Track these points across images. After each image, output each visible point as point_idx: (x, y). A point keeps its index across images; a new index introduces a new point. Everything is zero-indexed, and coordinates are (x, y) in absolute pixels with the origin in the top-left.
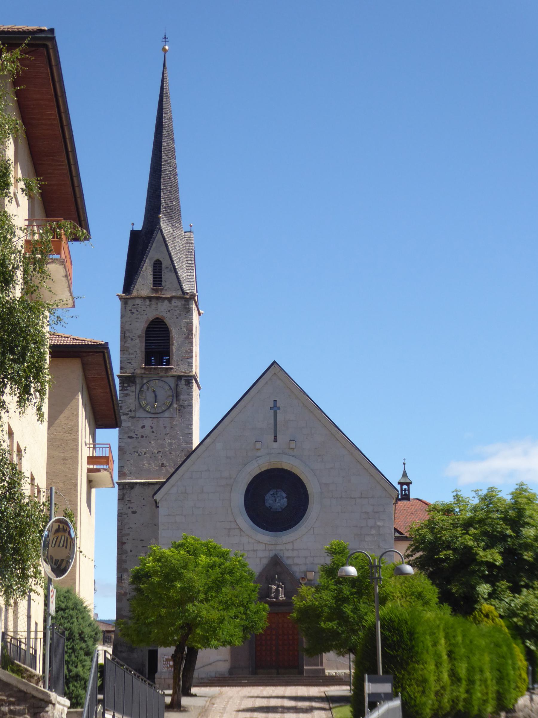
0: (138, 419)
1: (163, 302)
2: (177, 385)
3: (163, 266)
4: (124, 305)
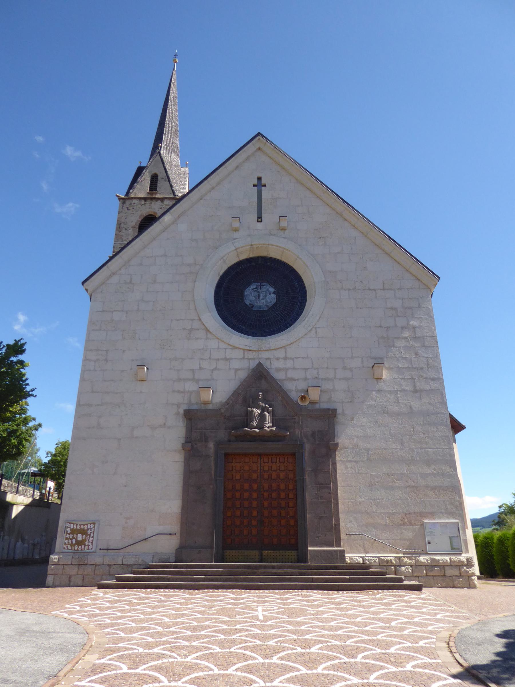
1: (156, 202)
4: (122, 204)
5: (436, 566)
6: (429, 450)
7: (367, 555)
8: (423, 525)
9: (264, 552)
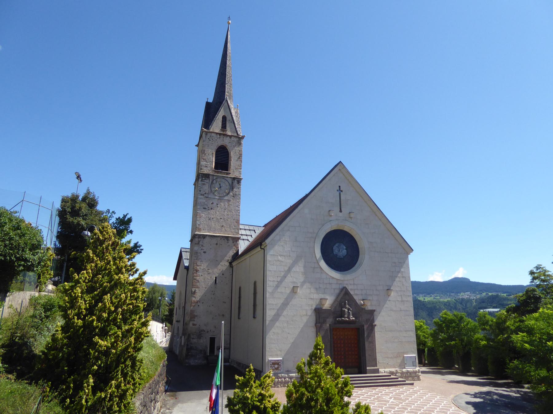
2: (233, 183)
5: (408, 373)
7: (386, 369)
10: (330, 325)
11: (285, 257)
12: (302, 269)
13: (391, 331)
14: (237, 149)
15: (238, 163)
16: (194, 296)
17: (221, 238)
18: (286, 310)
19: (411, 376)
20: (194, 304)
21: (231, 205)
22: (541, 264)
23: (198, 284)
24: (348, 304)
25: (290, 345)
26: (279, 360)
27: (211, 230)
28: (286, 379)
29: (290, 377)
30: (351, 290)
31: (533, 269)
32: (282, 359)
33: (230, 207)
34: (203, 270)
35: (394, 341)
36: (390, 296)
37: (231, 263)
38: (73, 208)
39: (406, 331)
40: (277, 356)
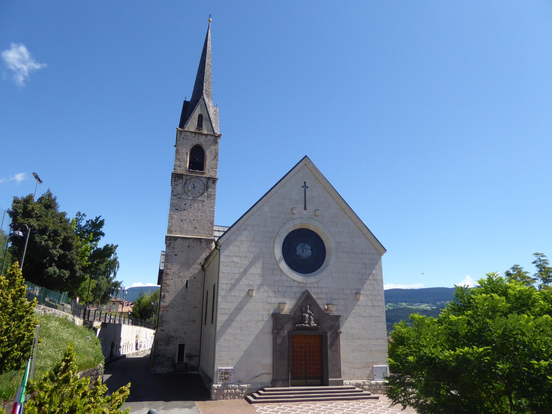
0: (182, 199)
1: (202, 136)
2: (207, 183)
3: (204, 118)
6: (377, 334)
8: (373, 367)
9: (307, 380)
10: (288, 332)
11: (241, 258)
12: (260, 272)
13: (359, 339)
14: (213, 148)
15: (214, 162)
16: (163, 300)
17: (193, 240)
18: (240, 316)
19: (381, 389)
20: (163, 309)
21: (205, 206)
22: (518, 264)
23: (168, 288)
24: (309, 309)
25: (243, 353)
26: (228, 370)
27: (183, 232)
28: (236, 390)
29: (241, 388)
30: (314, 293)
31: (509, 270)
32: (233, 368)
33: (203, 208)
34: (173, 273)
35: (362, 350)
36: (359, 301)
37: (203, 266)
38: (25, 208)
39: (376, 339)
40: (228, 364)
